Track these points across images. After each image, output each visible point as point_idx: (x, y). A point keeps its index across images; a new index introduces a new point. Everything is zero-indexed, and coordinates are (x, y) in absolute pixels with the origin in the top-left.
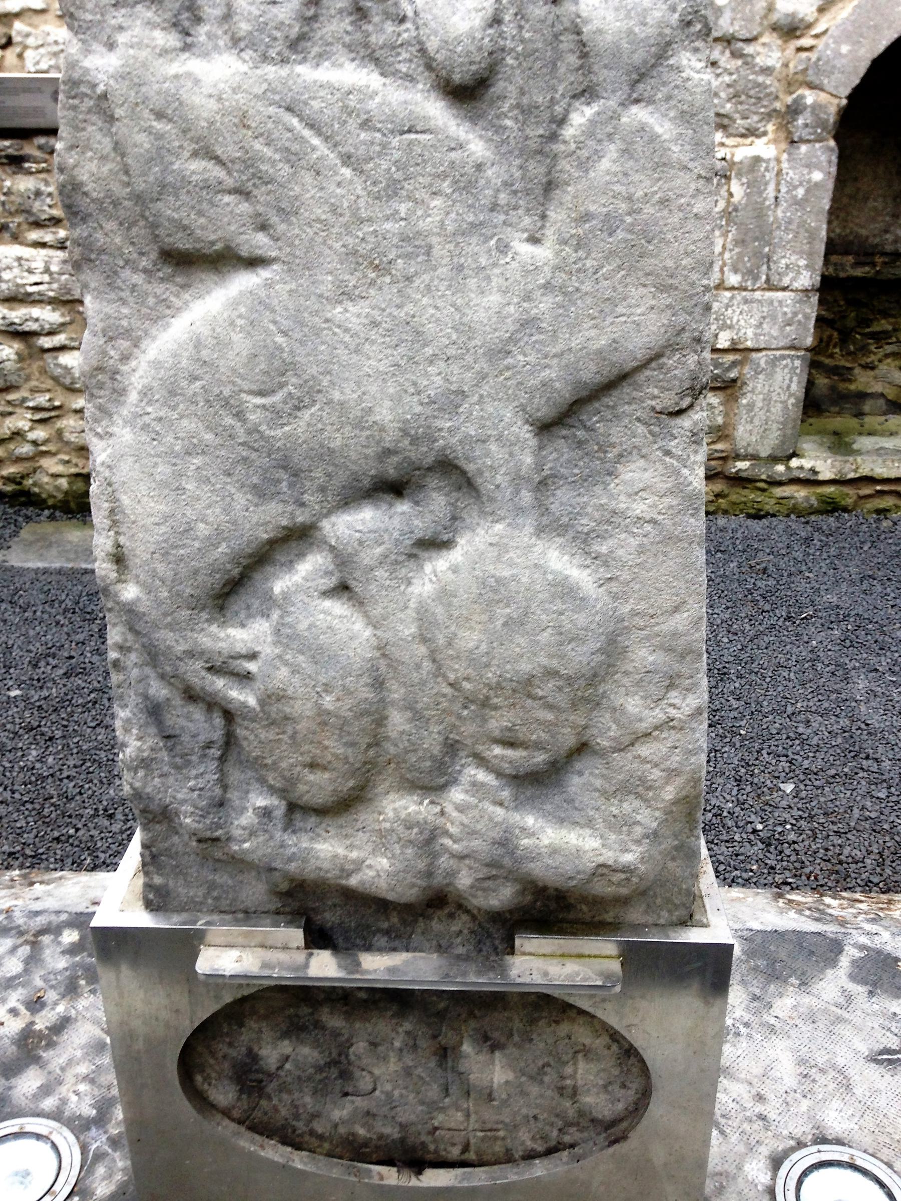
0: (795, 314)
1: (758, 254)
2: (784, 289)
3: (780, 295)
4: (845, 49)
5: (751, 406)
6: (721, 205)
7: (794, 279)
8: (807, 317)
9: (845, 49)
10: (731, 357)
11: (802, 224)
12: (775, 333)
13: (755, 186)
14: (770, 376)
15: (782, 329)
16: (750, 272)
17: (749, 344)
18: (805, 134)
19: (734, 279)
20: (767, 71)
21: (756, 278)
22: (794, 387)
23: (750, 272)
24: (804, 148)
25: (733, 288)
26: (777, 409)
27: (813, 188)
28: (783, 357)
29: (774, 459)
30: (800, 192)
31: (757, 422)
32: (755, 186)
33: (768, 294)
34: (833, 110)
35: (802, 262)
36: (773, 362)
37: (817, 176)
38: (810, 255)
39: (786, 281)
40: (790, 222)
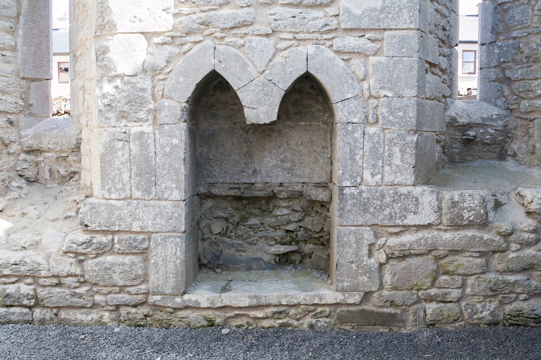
0: (173, 213)
1: (149, 181)
2: (166, 199)
3: (163, 203)
4: (181, 79)
5: (156, 264)
6: (127, 156)
7: (170, 194)
8: (180, 215)
9: (181, 79)
10: (140, 237)
11: (171, 165)
12: (163, 223)
13: (144, 146)
14: (165, 246)
15: (167, 221)
16: (146, 190)
17: (150, 229)
18: (166, 120)
19: (138, 194)
20: (143, 90)
21: (150, 193)
22: (178, 253)
23: (146, 190)
24: (166, 127)
25: (137, 199)
26: (171, 266)
27: (174, 147)
28: (170, 237)
29: (174, 295)
30: (168, 149)
31: (161, 273)
32: (144, 146)
33: (157, 202)
34: (179, 109)
35: (174, 186)
36: (165, 239)
37: (175, 141)
38: (177, 181)
39: (166, 195)
40: (164, 164)
